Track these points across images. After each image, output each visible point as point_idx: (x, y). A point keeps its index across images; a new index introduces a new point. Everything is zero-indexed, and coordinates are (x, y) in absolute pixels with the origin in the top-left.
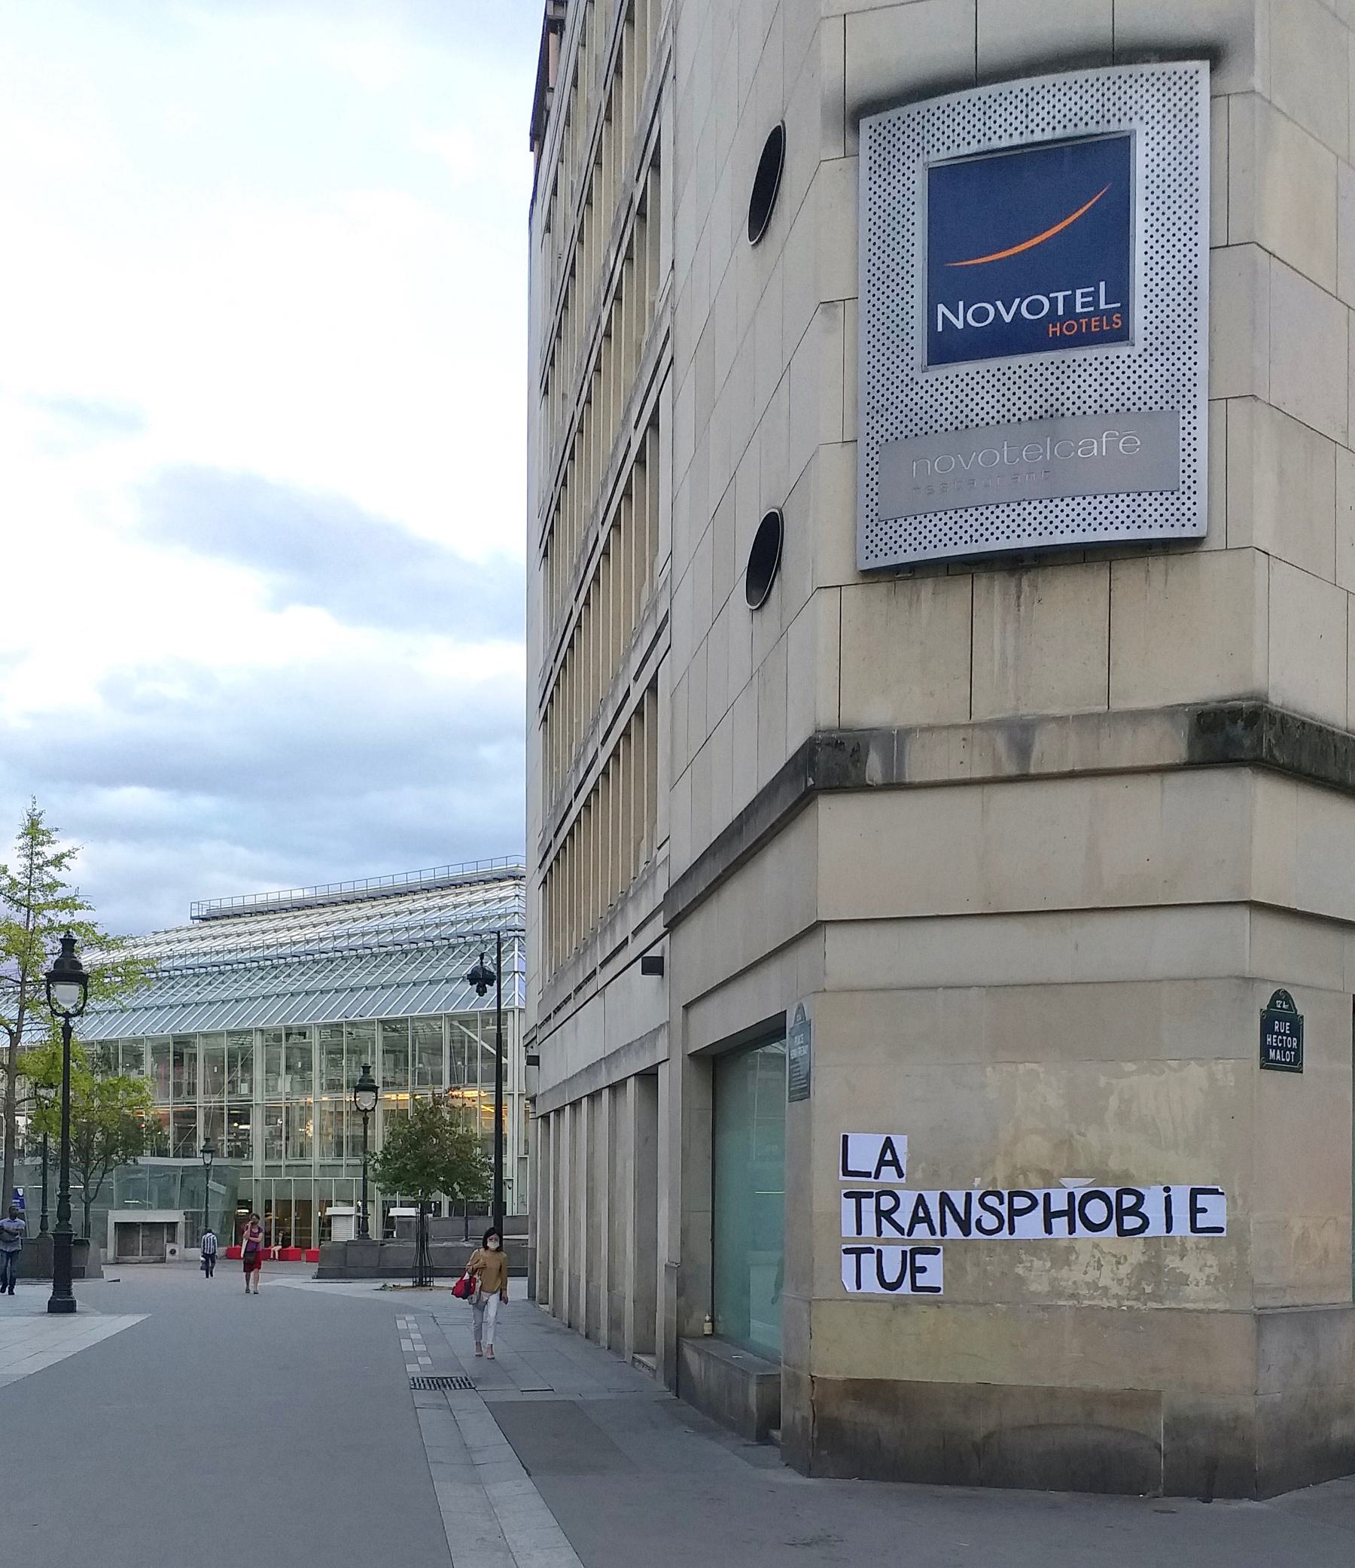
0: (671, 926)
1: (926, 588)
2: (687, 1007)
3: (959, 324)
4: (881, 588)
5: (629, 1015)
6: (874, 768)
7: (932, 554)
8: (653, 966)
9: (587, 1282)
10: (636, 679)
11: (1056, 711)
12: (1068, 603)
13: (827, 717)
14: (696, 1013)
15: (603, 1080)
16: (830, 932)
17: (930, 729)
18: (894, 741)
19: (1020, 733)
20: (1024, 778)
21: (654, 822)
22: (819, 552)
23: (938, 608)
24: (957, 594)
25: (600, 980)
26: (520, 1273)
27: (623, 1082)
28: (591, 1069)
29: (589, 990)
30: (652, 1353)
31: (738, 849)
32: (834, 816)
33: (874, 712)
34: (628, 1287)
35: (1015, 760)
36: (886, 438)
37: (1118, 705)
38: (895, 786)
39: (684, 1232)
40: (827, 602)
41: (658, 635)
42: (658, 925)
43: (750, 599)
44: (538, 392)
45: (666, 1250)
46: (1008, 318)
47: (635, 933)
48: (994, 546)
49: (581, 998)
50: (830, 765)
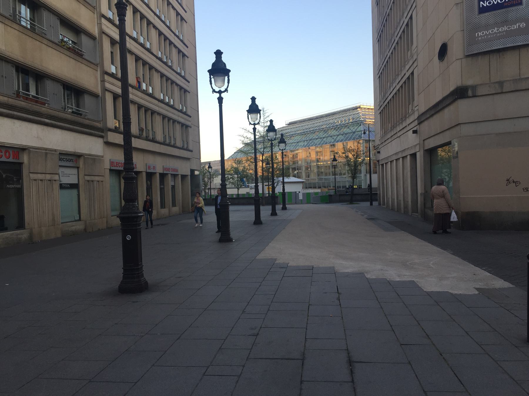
0: (419, 124)
1: (480, 57)
2: (424, 140)
3: (485, 5)
4: (469, 59)
5: (408, 141)
6: (470, 93)
7: (481, 51)
8: (415, 132)
9: (182, 192)
10: (407, 71)
11: (508, 79)
12: (510, 59)
13: (459, 84)
14: (426, 142)
15: (400, 155)
16: (461, 125)
17: (481, 85)
18: (474, 88)
19: (501, 84)
20: (502, 93)
21: (413, 100)
22: (456, 51)
23: (483, 61)
24: (486, 58)
25: (399, 134)
26: (376, 200)
27: (406, 156)
28: (396, 154)
29: (395, 136)
30: (417, 212)
31: (437, 108)
32: (462, 105)
33: (469, 82)
34: (401, 198)
35: (500, 89)
36: (470, 30)
37: (522, 77)
38: (474, 96)
39: (425, 186)
40: (459, 62)
41: (413, 63)
42: (416, 122)
43: (439, 59)
44: (375, 5)
45: (420, 190)
46: (495, 3)
47: (408, 125)
48: (494, 48)
49: (393, 138)
50: (460, 93)
